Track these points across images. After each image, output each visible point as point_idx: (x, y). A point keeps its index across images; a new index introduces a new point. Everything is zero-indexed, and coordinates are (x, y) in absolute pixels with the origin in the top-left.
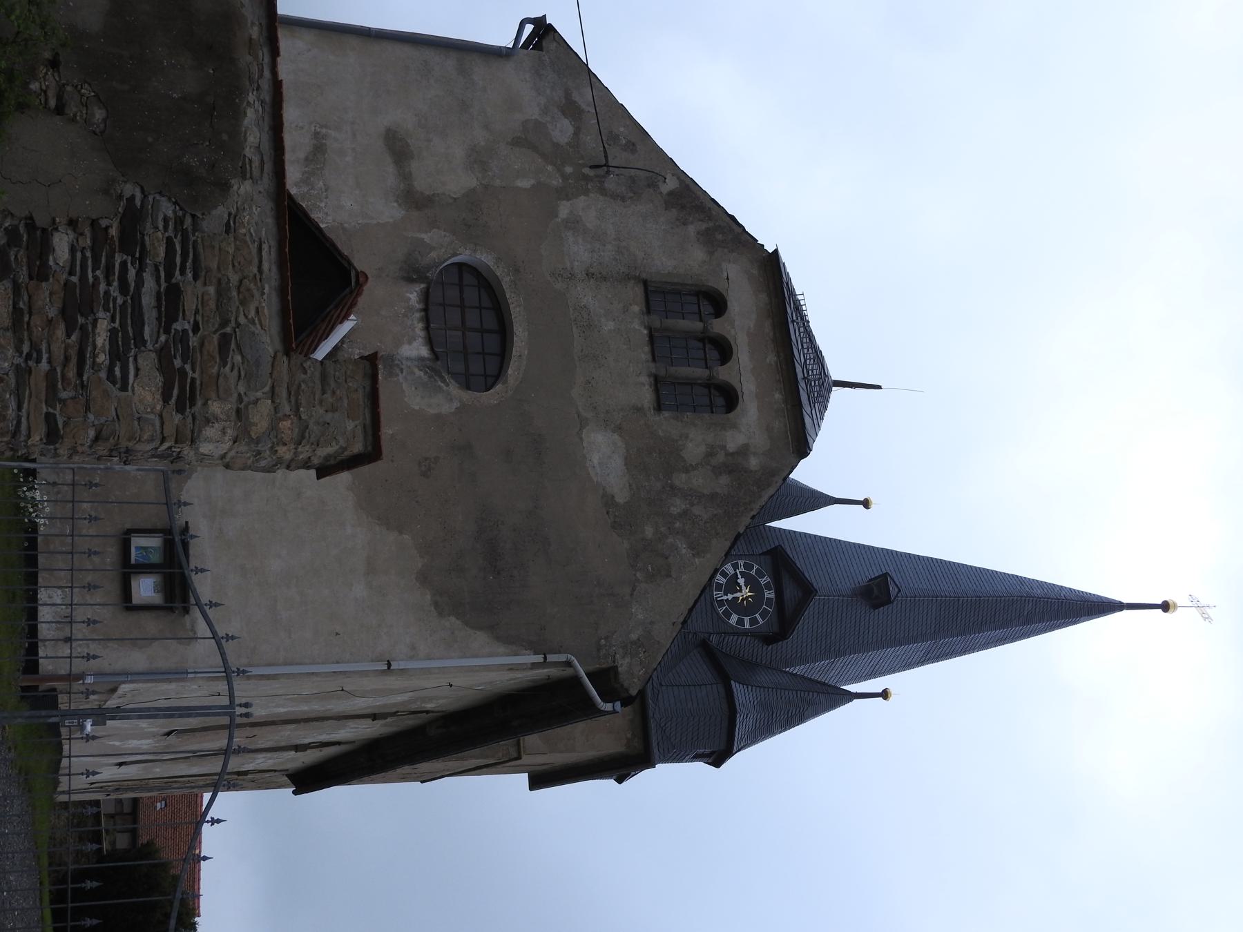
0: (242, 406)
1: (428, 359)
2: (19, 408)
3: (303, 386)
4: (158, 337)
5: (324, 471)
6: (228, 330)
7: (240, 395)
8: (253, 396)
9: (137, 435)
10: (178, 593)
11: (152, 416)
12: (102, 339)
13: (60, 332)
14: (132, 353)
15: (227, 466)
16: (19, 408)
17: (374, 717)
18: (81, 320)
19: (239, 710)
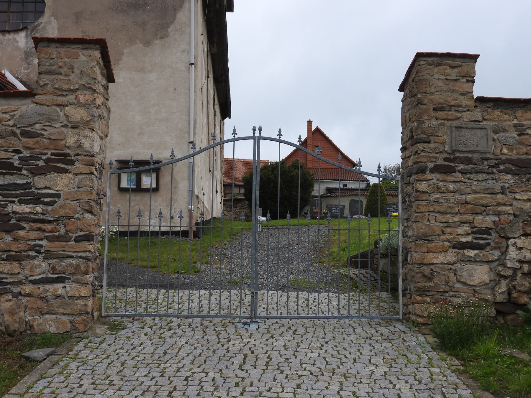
0: (70, 125)
1: (26, 33)
2: (72, 257)
3: (56, 86)
4: (24, 175)
5: (110, 79)
6: (18, 132)
7: (62, 126)
8: (63, 118)
9: (89, 189)
10: (153, 167)
11: (77, 180)
12: (26, 209)
13: (21, 233)
14: (35, 191)
15: (106, 136)
16: (72, 257)
17: (208, 77)
18: (13, 221)
19: (257, 134)
